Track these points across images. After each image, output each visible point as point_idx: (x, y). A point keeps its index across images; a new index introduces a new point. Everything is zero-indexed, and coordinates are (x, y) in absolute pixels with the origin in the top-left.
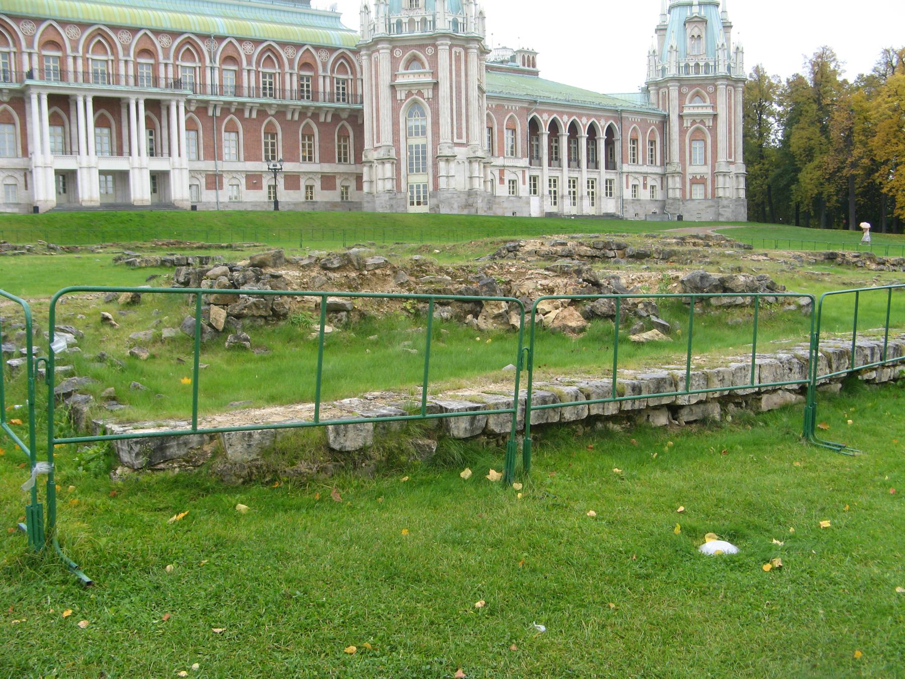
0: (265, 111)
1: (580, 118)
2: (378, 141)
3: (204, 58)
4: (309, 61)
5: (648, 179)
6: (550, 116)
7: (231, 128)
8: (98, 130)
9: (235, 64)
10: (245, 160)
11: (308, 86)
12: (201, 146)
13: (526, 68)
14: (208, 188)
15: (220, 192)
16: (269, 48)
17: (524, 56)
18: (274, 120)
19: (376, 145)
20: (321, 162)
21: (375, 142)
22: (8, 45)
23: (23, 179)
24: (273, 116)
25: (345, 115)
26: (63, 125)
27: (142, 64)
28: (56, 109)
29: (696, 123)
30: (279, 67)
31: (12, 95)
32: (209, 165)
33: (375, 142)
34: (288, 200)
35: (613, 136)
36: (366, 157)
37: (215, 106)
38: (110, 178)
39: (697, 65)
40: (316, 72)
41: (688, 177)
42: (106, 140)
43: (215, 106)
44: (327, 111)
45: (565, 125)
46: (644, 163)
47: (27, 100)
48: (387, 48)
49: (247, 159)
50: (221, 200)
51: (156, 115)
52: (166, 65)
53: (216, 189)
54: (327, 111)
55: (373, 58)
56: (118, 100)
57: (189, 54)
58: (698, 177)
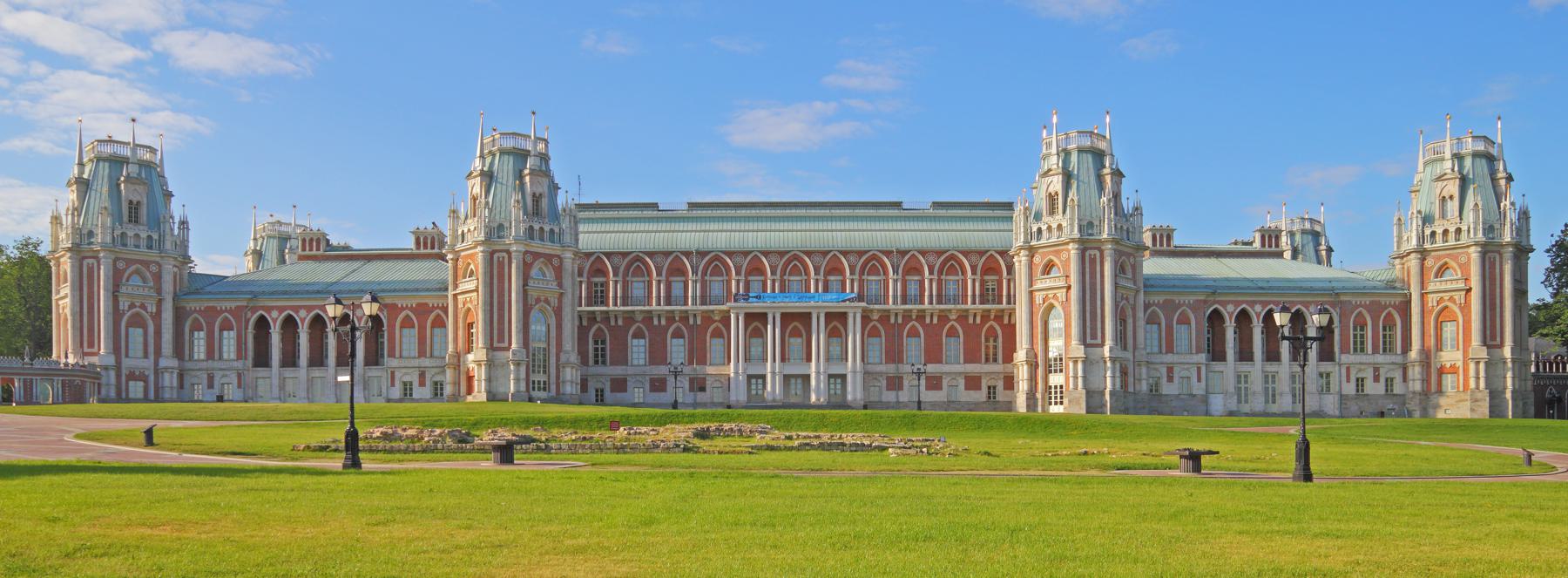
6: (1236, 306)
7: (678, 334)
9: (997, 275)
10: (965, 363)
15: (900, 393)
17: (1168, 245)
18: (876, 323)
20: (1004, 363)
21: (85, 344)
24: (955, 320)
25: (876, 317)
26: (841, 336)
29: (135, 307)
30: (963, 274)
31: (722, 315)
32: (890, 369)
33: (85, 344)
34: (968, 399)
35: (1252, 323)
37: (659, 317)
39: (1446, 232)
40: (845, 276)
41: (124, 372)
45: (1258, 316)
46: (1375, 350)
49: (966, 362)
50: (901, 400)
51: (804, 326)
52: (581, 282)
57: (716, 272)
58: (137, 373)
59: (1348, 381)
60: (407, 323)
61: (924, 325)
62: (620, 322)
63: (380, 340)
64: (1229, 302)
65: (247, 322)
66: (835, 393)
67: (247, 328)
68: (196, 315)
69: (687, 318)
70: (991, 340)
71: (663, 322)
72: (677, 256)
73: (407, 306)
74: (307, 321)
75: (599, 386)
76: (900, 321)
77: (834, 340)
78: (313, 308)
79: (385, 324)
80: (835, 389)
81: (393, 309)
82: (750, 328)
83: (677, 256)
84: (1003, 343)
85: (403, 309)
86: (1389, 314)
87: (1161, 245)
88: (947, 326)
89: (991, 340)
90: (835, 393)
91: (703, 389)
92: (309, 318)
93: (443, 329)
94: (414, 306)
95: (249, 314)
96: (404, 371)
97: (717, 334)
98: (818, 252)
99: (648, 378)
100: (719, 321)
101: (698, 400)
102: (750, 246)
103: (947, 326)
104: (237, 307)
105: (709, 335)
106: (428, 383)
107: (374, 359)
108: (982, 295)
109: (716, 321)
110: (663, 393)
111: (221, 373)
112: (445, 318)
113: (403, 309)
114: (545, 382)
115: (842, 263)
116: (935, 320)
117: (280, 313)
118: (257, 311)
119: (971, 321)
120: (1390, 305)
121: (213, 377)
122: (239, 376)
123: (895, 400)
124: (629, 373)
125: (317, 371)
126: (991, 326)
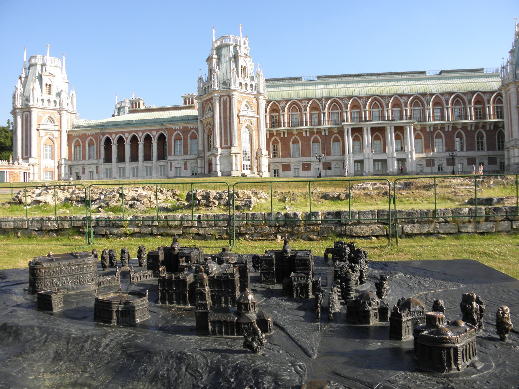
0: (498, 126)
1: (111, 135)
2: (512, 137)
3: (424, 104)
4: (480, 99)
5: (73, 169)
7: (316, 141)
8: (396, 141)
9: (440, 106)
11: (480, 112)
12: (423, 146)
13: (187, 105)
14: (427, 166)
15: (433, 168)
16: (294, 103)
19: (511, 139)
21: (24, 154)
22: (379, 108)
23: (342, 165)
25: (295, 132)
26: (360, 140)
27: (314, 114)
28: (398, 132)
36: (506, 146)
38: (380, 163)
42: (420, 144)
43: (306, 132)
44: (449, 125)
47: (404, 129)
48: (514, 88)
51: (381, 134)
53: (431, 166)
54: (491, 124)
55: (508, 94)
56: (384, 127)
59: (171, 170)
60: (178, 138)
61: (444, 132)
62: (286, 136)
63: (165, 148)
64: (126, 132)
65: (101, 140)
66: (358, 170)
67: (100, 144)
68: (77, 138)
69: (321, 132)
70: (500, 138)
71: (308, 134)
72: (396, 97)
73: (193, 127)
74: (128, 139)
75: (276, 168)
76: (432, 130)
77: (357, 143)
78: (146, 131)
79: (167, 139)
80: (358, 168)
81: (171, 131)
82: (373, 137)
83: (396, 97)
84: (487, 140)
85: (175, 130)
86: (91, 140)
87: (136, 107)
88: (457, 132)
89: (500, 138)
90: (358, 170)
91: (330, 168)
92: (143, 136)
93: (196, 140)
94: (181, 128)
95: (102, 136)
96: (176, 162)
97: (336, 140)
98: (364, 97)
99: (301, 164)
100: (337, 133)
101: (328, 174)
102: (351, 94)
103: (457, 132)
104: (96, 134)
105: (332, 140)
106: (188, 168)
107: (162, 156)
108: (270, 124)
109: (335, 133)
110: (309, 171)
111: (89, 166)
112: (197, 134)
113: (175, 130)
114: (250, 166)
115: (400, 101)
116: (450, 129)
117: (143, 133)
118: (105, 135)
119: (282, 136)
120: (91, 135)
121: (85, 169)
122: (97, 167)
123: (431, 172)
124: (292, 161)
125: (134, 164)
126: (439, 133)
